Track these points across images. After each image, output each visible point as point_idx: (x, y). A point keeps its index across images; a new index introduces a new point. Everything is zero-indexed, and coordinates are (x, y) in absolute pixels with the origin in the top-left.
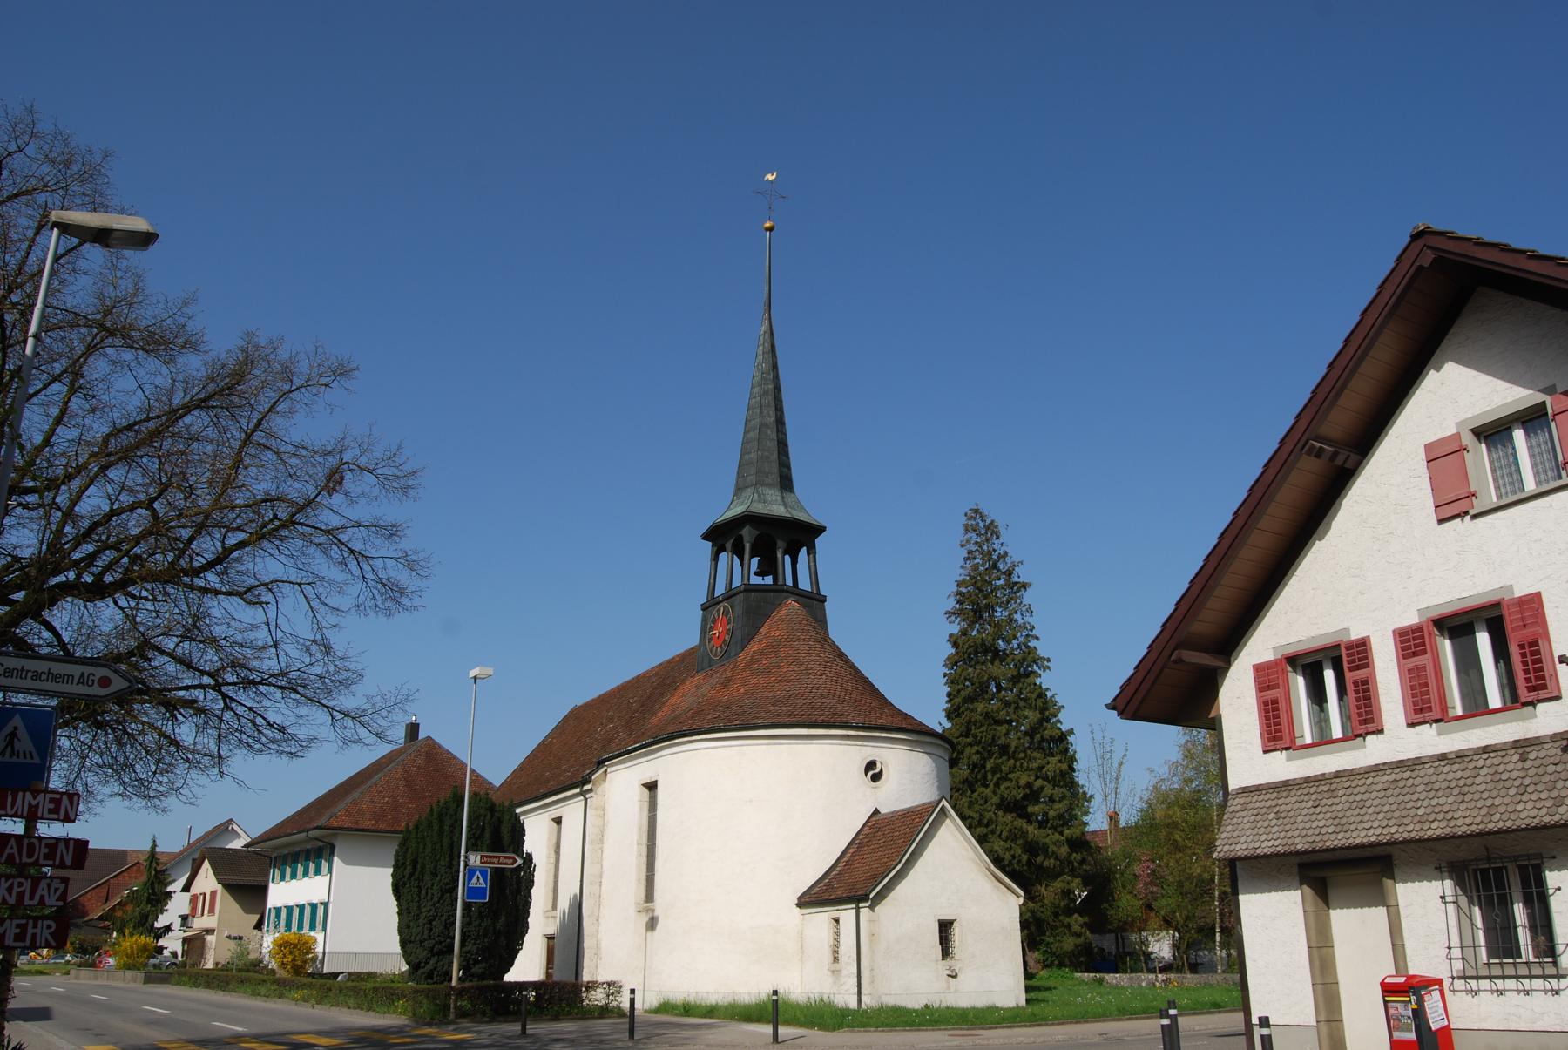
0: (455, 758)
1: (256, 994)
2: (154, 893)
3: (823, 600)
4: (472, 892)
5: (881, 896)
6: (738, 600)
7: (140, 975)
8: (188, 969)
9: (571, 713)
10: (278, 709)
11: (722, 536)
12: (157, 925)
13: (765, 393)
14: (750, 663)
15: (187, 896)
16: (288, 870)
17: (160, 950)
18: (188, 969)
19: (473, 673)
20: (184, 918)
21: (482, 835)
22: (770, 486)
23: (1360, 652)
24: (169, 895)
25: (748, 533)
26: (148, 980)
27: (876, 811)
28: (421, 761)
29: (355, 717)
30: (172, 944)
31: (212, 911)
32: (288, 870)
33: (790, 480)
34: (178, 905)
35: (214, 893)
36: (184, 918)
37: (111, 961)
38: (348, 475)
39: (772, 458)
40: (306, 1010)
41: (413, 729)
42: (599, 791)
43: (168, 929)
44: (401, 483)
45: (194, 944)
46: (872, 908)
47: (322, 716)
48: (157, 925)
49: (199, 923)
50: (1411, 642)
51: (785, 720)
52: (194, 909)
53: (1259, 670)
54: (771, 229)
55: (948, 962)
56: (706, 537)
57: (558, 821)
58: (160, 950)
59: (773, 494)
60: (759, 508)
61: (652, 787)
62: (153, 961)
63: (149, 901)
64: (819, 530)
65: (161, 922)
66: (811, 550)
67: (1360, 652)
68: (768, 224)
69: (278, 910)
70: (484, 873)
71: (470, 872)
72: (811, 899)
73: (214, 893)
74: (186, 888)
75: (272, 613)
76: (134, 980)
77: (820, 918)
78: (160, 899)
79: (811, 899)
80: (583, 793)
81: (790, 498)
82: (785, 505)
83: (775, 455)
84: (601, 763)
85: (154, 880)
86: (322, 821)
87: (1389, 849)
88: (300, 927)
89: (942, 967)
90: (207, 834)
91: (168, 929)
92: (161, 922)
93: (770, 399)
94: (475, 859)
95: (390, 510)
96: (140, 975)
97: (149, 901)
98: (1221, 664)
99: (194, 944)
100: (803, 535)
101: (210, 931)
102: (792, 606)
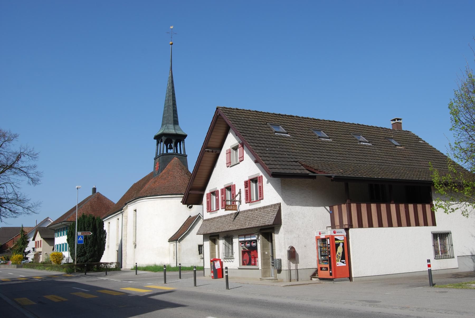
0: (106, 198)
1: (40, 269)
2: (24, 241)
3: (186, 156)
4: (79, 242)
5: (182, 239)
6: (160, 157)
7: (16, 266)
8: (35, 264)
9: (132, 188)
10: (14, 207)
11: (158, 138)
12: (25, 251)
13: (170, 96)
14: (162, 176)
15: (34, 242)
16: (59, 233)
17: (27, 258)
18: (35, 264)
19: (77, 187)
20: (34, 249)
21: (90, 226)
22: (171, 124)
23: (218, 191)
24: (28, 242)
25: (164, 138)
26: (18, 267)
27: (190, 216)
28: (96, 200)
29: (28, 208)
30: (31, 257)
31: (41, 246)
32: (59, 233)
33: (178, 122)
34: (31, 245)
35: (41, 241)
36: (34, 249)
37: (11, 262)
38: (22, 156)
39: (172, 115)
40: (40, 271)
41: (94, 190)
42: (125, 211)
43: (29, 252)
44: (34, 156)
45: (37, 256)
46: (179, 242)
47: (21, 208)
48: (25, 251)
49: (38, 250)
50: (222, 190)
51: (165, 193)
52: (36, 246)
53: (207, 194)
54: (172, 44)
55: (202, 255)
56: (155, 138)
57: (118, 219)
58: (27, 258)
59: (171, 126)
60: (167, 131)
61: (135, 211)
62: (23, 262)
63: (22, 244)
64: (185, 136)
65: (27, 250)
66: (184, 143)
67: (218, 191)
68: (171, 43)
69: (58, 245)
70: (82, 237)
71: (79, 237)
72: (171, 240)
73: (41, 241)
74: (34, 240)
75: (5, 189)
76: (14, 267)
77: (172, 245)
78: (25, 243)
79: (171, 240)
80: (121, 213)
81: (177, 127)
82: (175, 130)
83: (172, 114)
84: (126, 204)
85: (23, 237)
86: (65, 220)
87: (273, 226)
88: (60, 251)
89: (199, 257)
90: (41, 222)
91: (29, 252)
92: (27, 250)
93: (171, 97)
94: (80, 233)
95: (32, 163)
96: (16, 266)
97: (22, 244)
98: (202, 193)
99: (37, 256)
100: (181, 138)
101: (40, 252)
102: (176, 159)
